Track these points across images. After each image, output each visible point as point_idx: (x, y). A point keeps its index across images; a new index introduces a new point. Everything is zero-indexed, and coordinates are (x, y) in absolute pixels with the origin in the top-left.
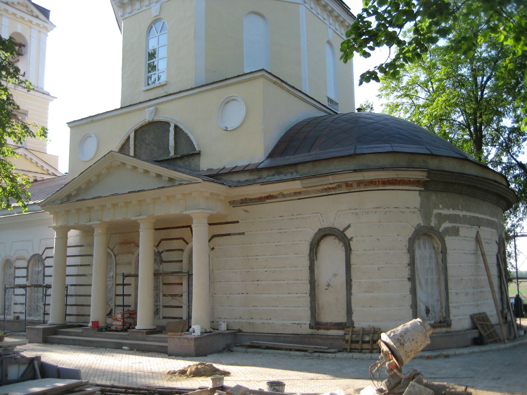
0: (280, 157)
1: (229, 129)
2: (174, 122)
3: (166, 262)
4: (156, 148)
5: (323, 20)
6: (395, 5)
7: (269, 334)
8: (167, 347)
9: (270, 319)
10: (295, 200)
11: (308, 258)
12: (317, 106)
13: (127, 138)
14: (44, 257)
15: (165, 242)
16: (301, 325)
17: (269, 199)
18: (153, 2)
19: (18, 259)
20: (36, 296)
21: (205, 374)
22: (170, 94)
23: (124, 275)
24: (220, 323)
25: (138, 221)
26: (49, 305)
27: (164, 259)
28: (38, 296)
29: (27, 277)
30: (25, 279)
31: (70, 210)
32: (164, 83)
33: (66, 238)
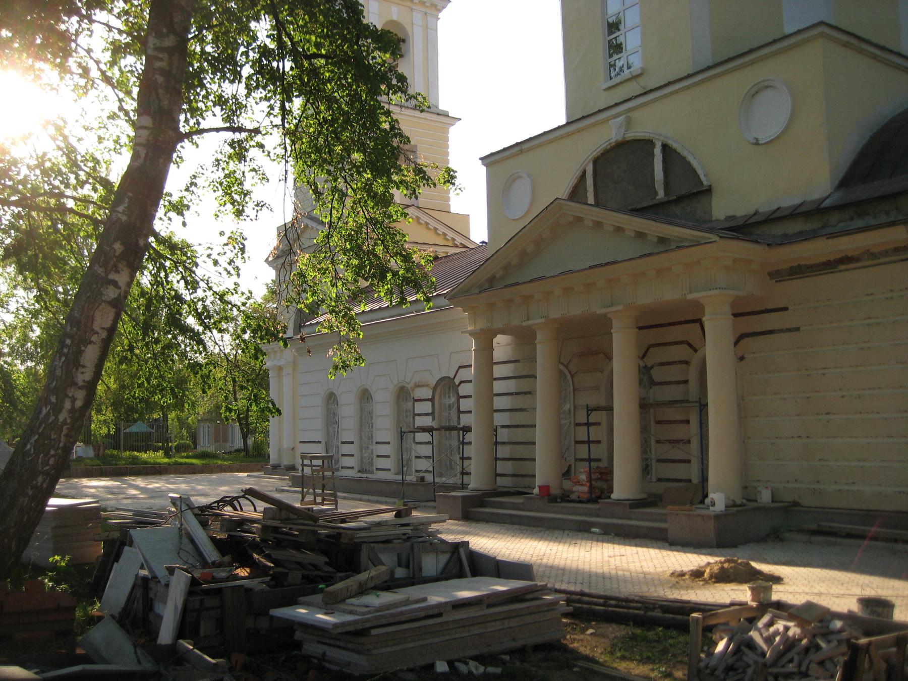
2: (662, 138)
3: (660, 384)
8: (666, 530)
14: (457, 381)
15: (656, 349)
19: (417, 386)
27: (656, 380)
29: (433, 414)
32: (639, 72)
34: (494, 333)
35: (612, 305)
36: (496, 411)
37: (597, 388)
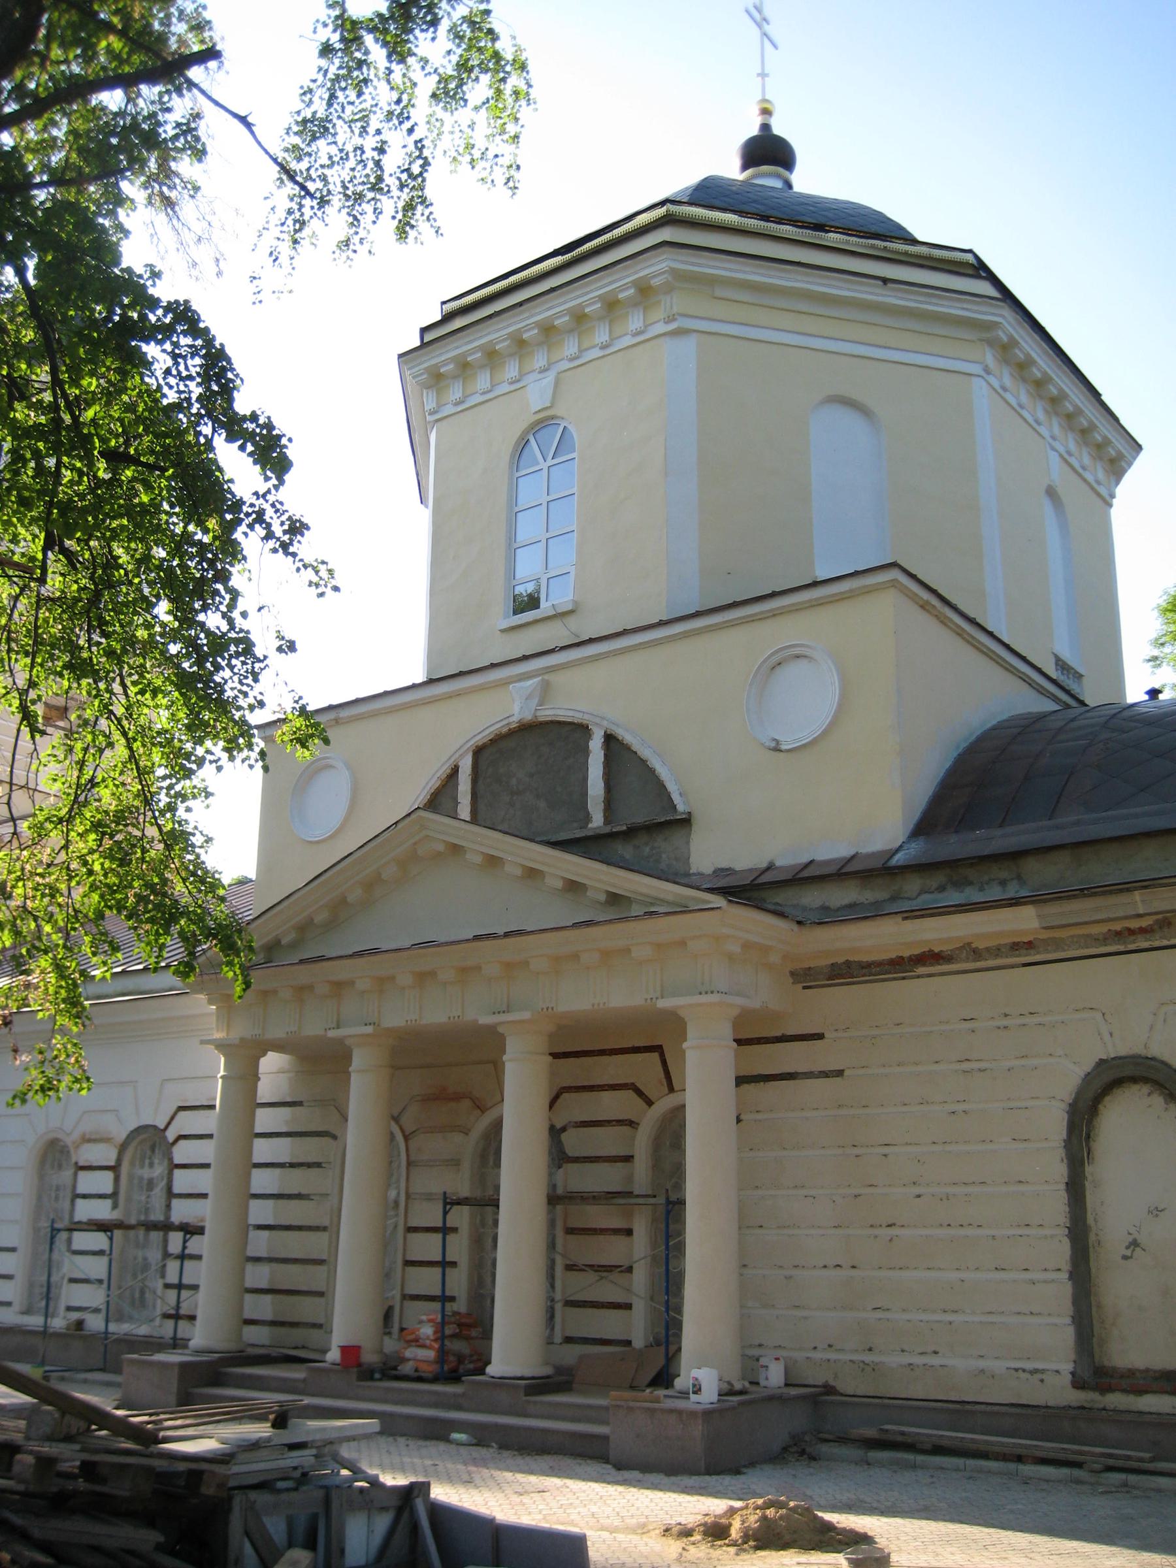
0: (956, 832)
1: (784, 747)
2: (605, 723)
3: (576, 1160)
4: (542, 804)
5: (1035, 425)
6: (305, 531)
7: (939, 1404)
8: (605, 1438)
9: (936, 1353)
10: (1012, 967)
11: (1061, 1152)
12: (1033, 681)
13: (449, 771)
14: (171, 1135)
15: (573, 1095)
16: (1044, 1377)
17: (924, 965)
18: (534, 371)
20: (140, 1259)
21: (795, 1541)
22: (591, 641)
23: (448, 1200)
24: (763, 1361)
25: (500, 1030)
26: (195, 1288)
27: (571, 1153)
28: (145, 1259)
29: (114, 1196)
30: (108, 1203)
31: (275, 992)
32: (570, 608)
33: (254, 1076)
34: (265, 1047)
35: (508, 1010)
36: (256, 1196)
37: (455, 1163)
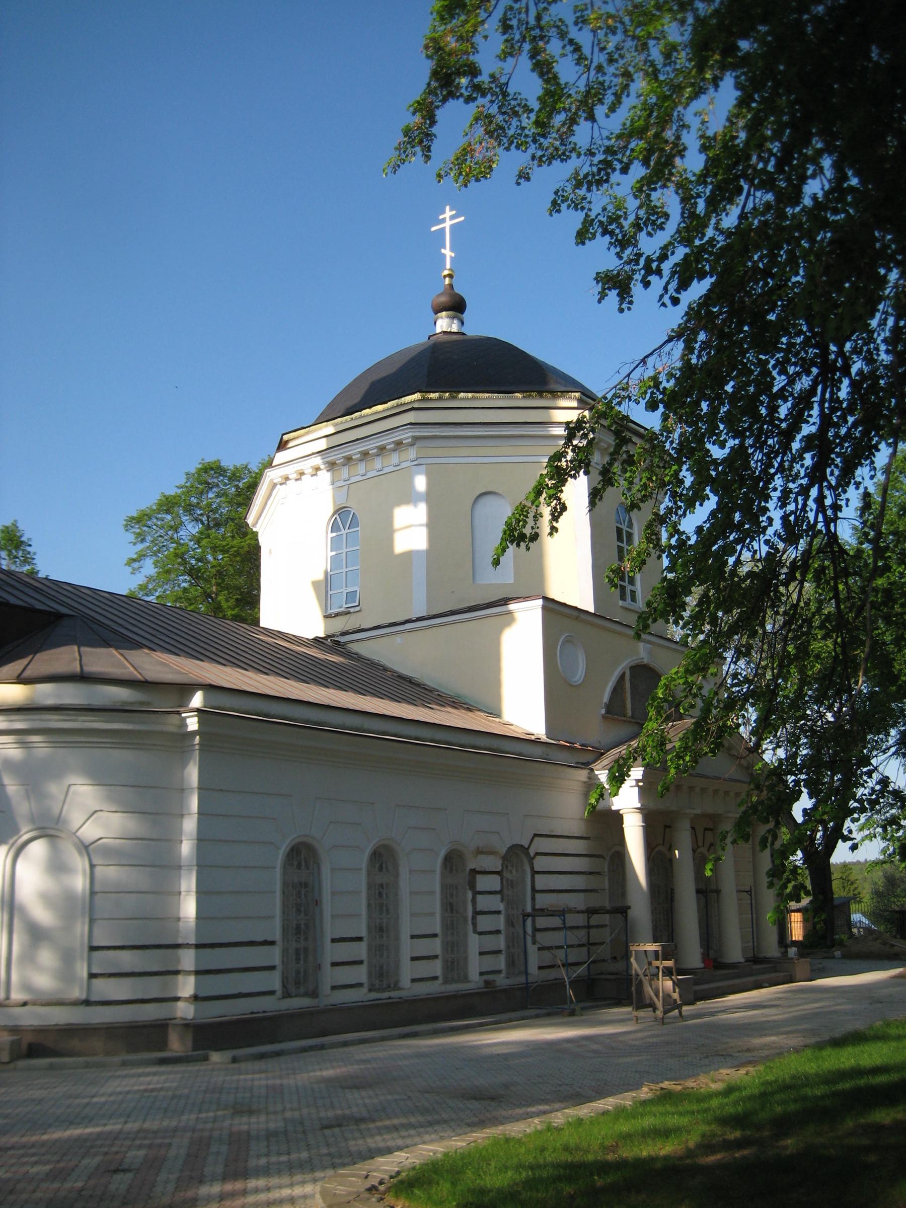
19: (479, 852)
30: (499, 897)
